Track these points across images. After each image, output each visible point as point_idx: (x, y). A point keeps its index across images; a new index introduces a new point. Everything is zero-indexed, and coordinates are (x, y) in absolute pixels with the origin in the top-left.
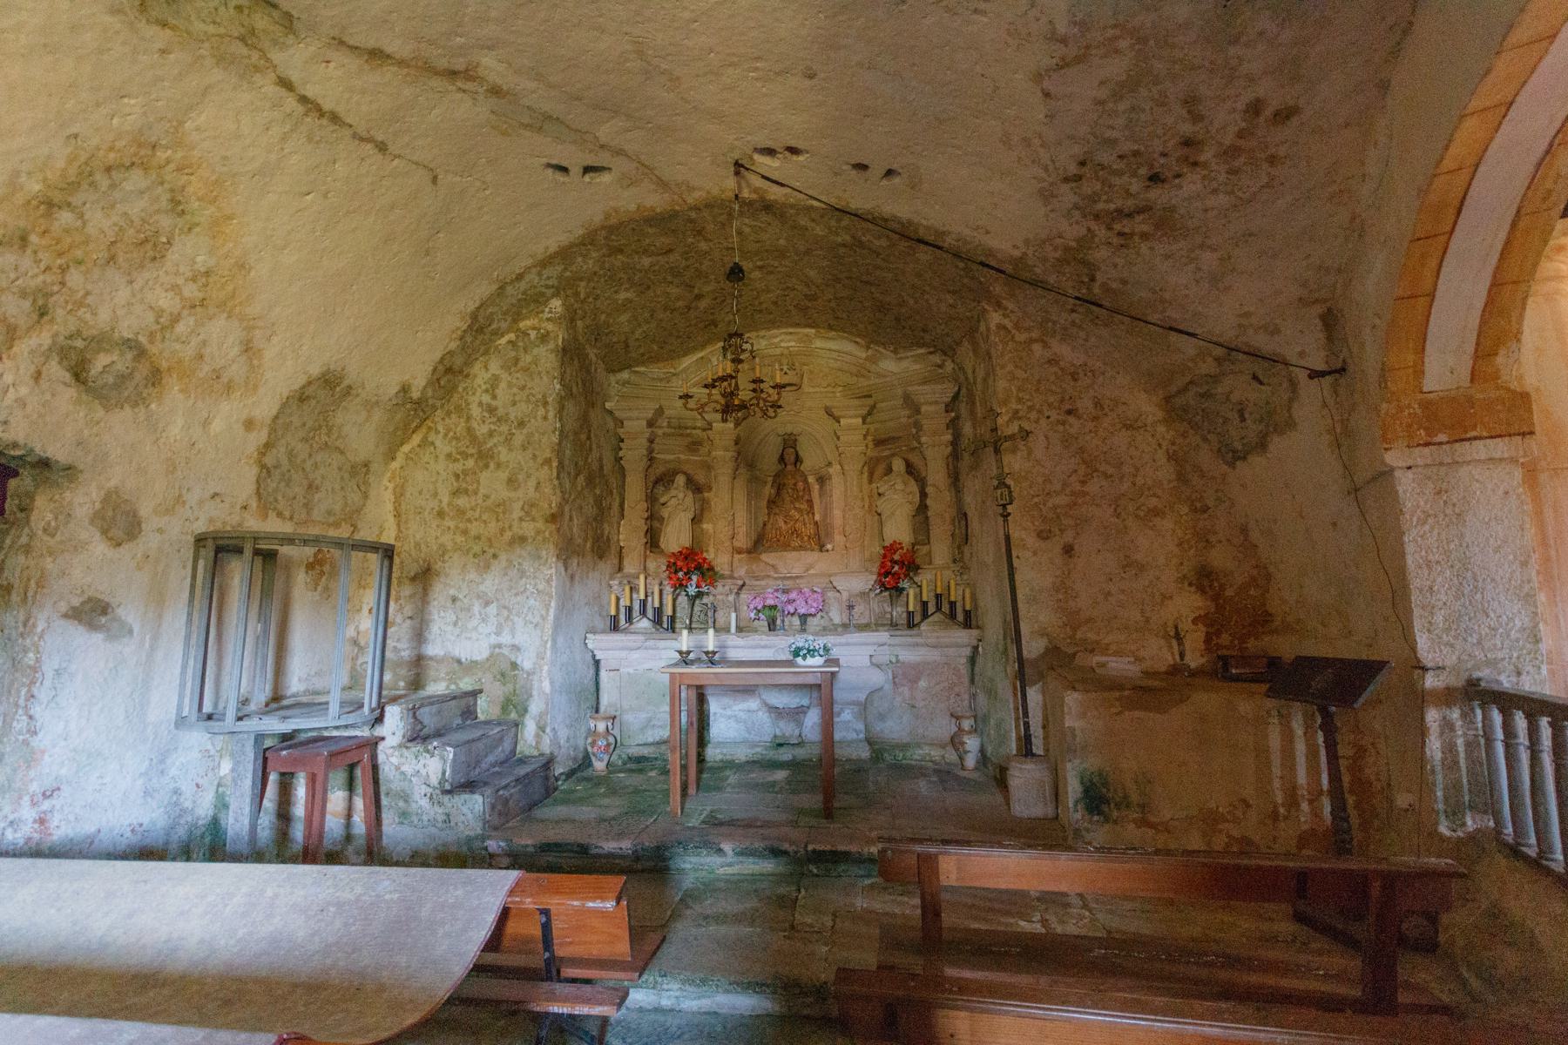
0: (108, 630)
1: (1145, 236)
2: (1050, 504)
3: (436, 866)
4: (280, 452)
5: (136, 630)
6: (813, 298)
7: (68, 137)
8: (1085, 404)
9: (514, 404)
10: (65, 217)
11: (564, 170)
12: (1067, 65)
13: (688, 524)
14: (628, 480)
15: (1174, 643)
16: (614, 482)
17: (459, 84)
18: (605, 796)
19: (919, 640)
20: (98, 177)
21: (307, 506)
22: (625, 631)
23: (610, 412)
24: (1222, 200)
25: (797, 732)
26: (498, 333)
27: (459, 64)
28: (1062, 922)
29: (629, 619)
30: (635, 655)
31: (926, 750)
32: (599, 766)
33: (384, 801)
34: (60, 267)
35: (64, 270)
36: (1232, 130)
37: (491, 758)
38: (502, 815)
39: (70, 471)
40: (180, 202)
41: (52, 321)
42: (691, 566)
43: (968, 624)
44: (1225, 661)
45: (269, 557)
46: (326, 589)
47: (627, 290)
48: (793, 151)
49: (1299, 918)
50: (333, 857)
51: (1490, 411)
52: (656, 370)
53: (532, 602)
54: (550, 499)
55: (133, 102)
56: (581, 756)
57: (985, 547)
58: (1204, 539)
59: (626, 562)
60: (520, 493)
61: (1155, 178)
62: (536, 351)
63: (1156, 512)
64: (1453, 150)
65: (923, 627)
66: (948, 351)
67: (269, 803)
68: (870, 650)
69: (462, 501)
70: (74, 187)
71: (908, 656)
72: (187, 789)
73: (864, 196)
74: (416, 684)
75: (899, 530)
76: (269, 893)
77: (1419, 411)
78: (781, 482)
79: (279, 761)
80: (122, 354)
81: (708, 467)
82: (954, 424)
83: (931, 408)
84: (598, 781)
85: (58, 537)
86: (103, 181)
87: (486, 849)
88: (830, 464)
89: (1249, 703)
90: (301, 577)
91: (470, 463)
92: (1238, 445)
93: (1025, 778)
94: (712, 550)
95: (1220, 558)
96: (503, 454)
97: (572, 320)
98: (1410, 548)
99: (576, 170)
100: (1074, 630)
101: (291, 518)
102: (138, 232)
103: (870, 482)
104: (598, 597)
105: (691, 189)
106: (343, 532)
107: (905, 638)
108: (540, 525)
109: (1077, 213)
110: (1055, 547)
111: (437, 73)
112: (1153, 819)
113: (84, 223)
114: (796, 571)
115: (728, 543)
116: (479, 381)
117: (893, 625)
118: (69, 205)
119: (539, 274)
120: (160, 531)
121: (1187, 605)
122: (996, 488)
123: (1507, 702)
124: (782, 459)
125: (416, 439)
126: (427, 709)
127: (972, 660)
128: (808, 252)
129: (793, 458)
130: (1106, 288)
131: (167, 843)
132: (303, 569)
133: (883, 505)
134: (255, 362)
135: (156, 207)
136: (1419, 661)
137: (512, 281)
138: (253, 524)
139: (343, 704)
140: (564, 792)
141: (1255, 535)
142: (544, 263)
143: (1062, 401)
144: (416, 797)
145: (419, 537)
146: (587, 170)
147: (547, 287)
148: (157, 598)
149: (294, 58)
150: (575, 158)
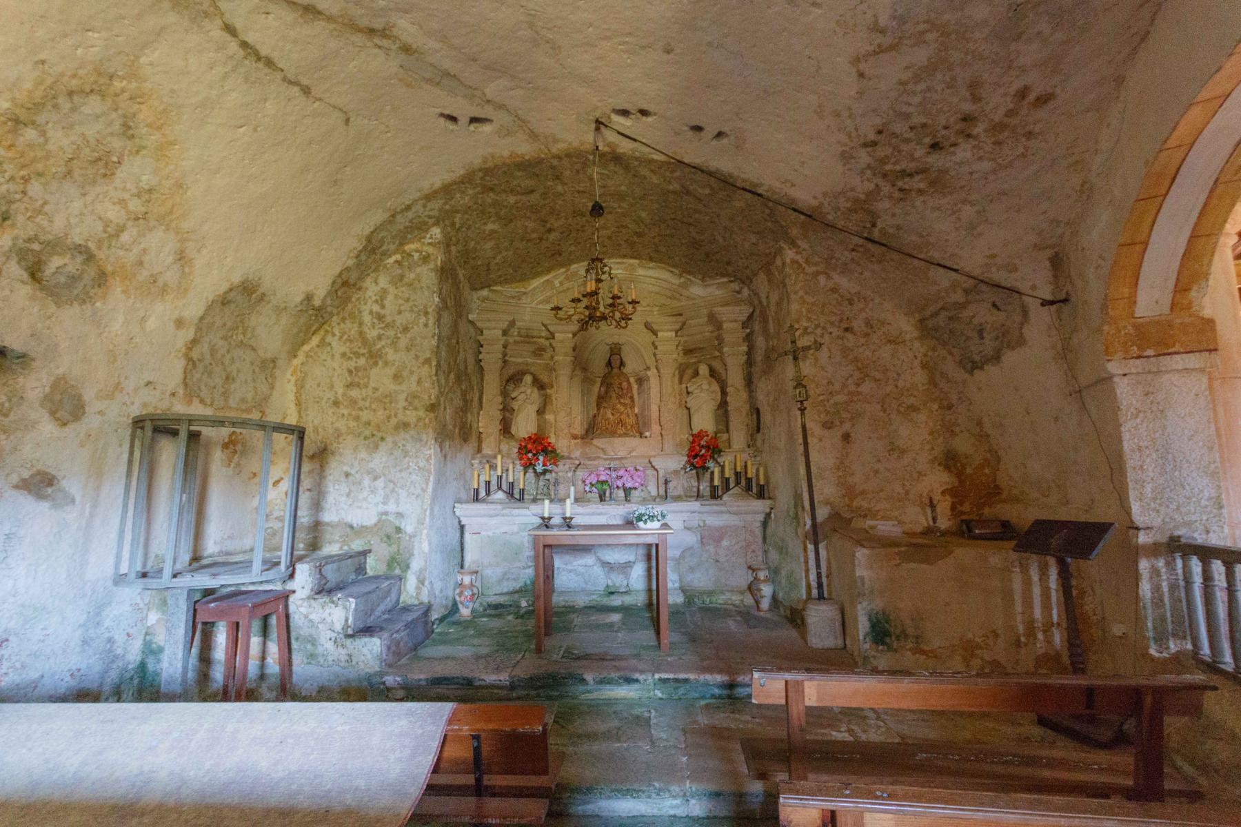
0: (53, 499)
1: (921, 192)
2: (832, 401)
3: (340, 701)
4: (204, 348)
5: (78, 499)
6: (640, 235)
7: (36, 63)
8: (858, 324)
9: (400, 312)
10: (30, 134)
11: (453, 119)
12: (882, 51)
13: (534, 415)
14: (486, 378)
15: (929, 511)
16: (475, 380)
17: (377, 41)
18: (474, 636)
19: (723, 508)
20: (61, 100)
21: (226, 395)
22: (483, 501)
23: (472, 322)
24: (986, 165)
25: (625, 583)
26: (386, 254)
27: (378, 24)
28: (865, 731)
29: (488, 493)
30: (494, 521)
31: (728, 595)
32: (465, 612)
33: (295, 645)
34: (23, 178)
35: (26, 180)
36: (1001, 111)
37: (382, 607)
38: (395, 654)
39: (24, 358)
40: (130, 128)
41: (13, 226)
42: (537, 449)
43: (761, 494)
44: (967, 523)
45: (194, 437)
46: (238, 465)
47: (494, 222)
48: (644, 113)
49: (1042, 722)
50: (249, 695)
51: (1182, 334)
52: (509, 290)
53: (414, 477)
54: (430, 392)
55: (96, 35)
56: (450, 604)
57: (778, 431)
58: (950, 430)
59: (484, 446)
60: (404, 387)
61: (935, 146)
62: (418, 270)
63: (914, 409)
64: (1176, 133)
65: (725, 498)
66: (746, 280)
67: (195, 651)
68: (685, 516)
69: (355, 393)
70: (38, 107)
71: (714, 521)
72: (120, 638)
73: (694, 152)
74: (314, 546)
75: (705, 421)
76: (230, 728)
77: (1132, 331)
78: (609, 382)
79: (204, 613)
80: (73, 257)
81: (552, 369)
82: (749, 338)
83: (731, 325)
84: (464, 624)
85: (12, 417)
86: (65, 104)
87: (384, 683)
88: (648, 368)
89: (998, 556)
90: (218, 455)
91: (362, 361)
92: (977, 358)
93: (820, 618)
94: (552, 435)
95: (963, 444)
96: (391, 355)
97: (448, 246)
98: (1126, 437)
99: (463, 120)
100: (852, 500)
101: (212, 405)
102: (94, 151)
103: (680, 383)
104: (462, 475)
105: (556, 141)
106: (255, 416)
107: (713, 506)
108: (421, 413)
109: (869, 172)
110: (838, 432)
111: (359, 30)
112: (926, 648)
113: (47, 141)
114: (621, 454)
115: (566, 431)
116: (369, 293)
117: (699, 496)
118: (33, 123)
119: (424, 206)
120: (101, 413)
121: (937, 480)
122: (795, 388)
123: (1206, 553)
124: (609, 364)
125: (316, 340)
126: (329, 567)
127: (765, 524)
128: (642, 198)
129: (618, 363)
130: (882, 231)
131: (101, 685)
132: (219, 449)
133: (692, 402)
134: (187, 270)
135: (110, 130)
136: (1132, 522)
137: (402, 211)
138: (180, 408)
139: (264, 562)
140: (440, 634)
141: (987, 427)
142: (428, 198)
143: (841, 321)
144: (323, 641)
145: (318, 421)
146: (474, 120)
147: (430, 217)
148: (97, 472)
150: (464, 109)
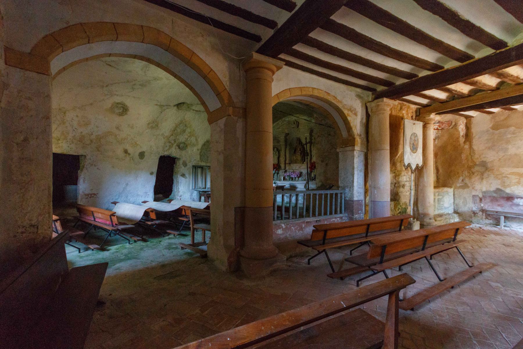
148: (189, 174)
149: (194, 108)
